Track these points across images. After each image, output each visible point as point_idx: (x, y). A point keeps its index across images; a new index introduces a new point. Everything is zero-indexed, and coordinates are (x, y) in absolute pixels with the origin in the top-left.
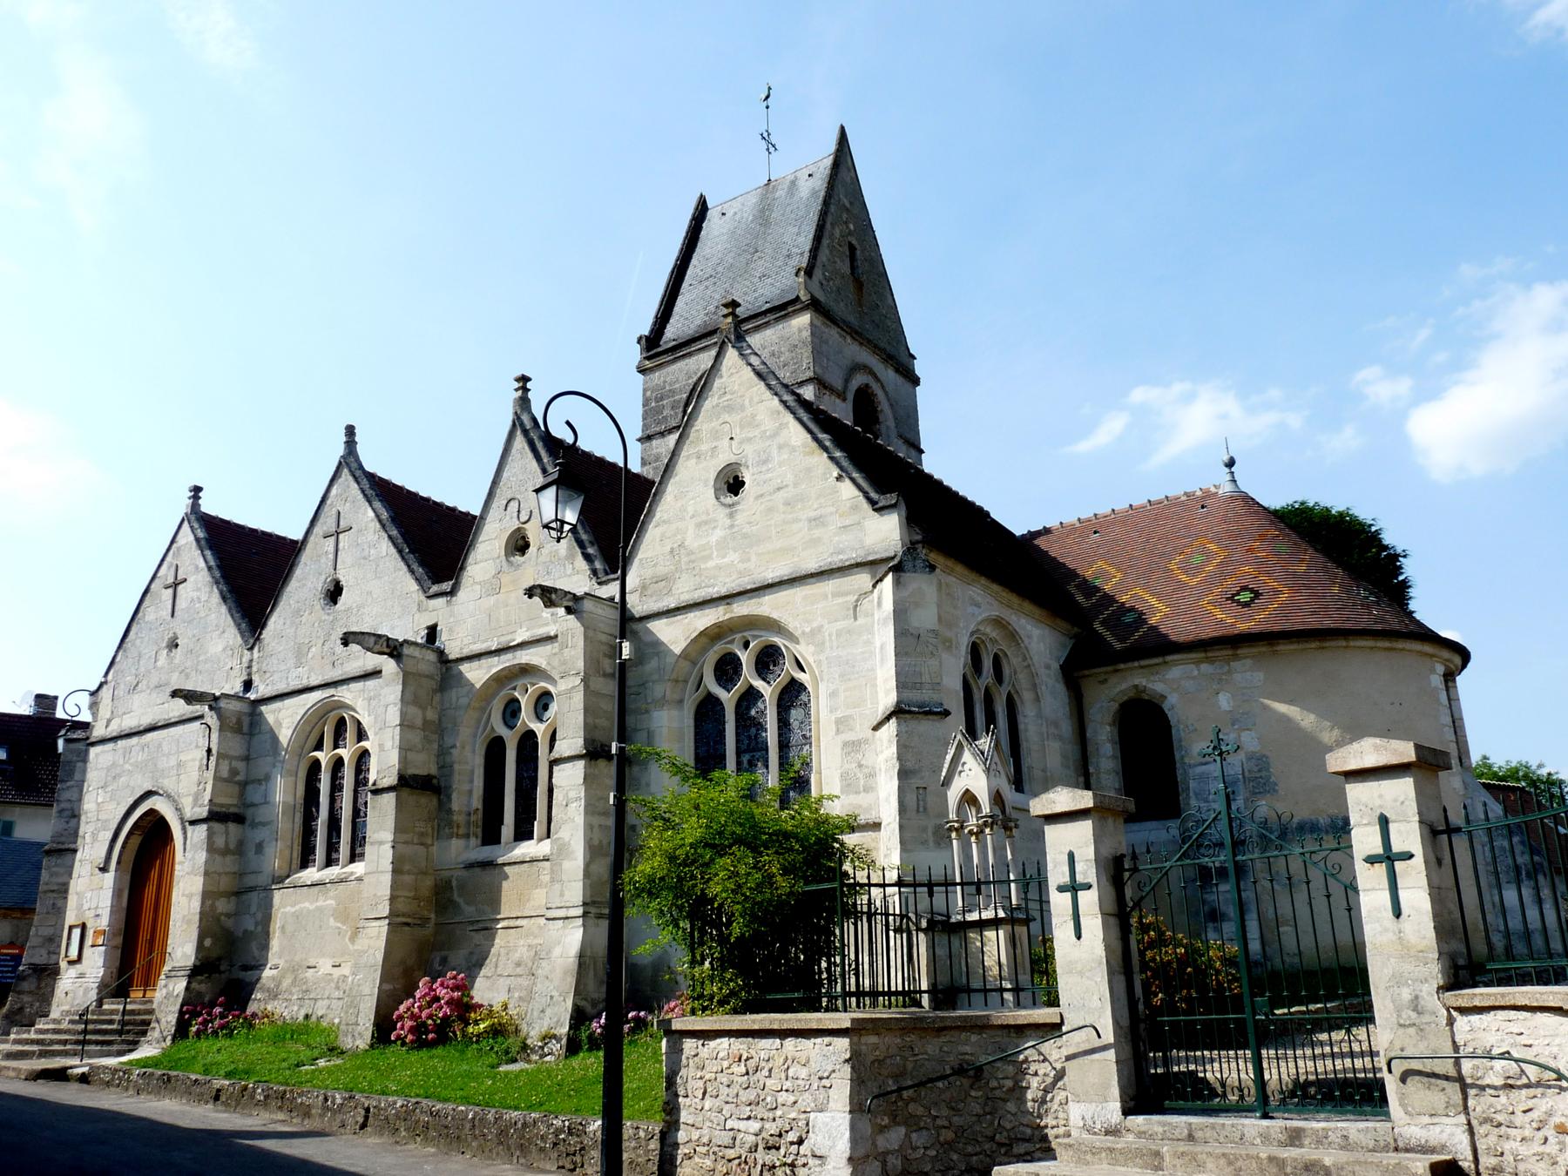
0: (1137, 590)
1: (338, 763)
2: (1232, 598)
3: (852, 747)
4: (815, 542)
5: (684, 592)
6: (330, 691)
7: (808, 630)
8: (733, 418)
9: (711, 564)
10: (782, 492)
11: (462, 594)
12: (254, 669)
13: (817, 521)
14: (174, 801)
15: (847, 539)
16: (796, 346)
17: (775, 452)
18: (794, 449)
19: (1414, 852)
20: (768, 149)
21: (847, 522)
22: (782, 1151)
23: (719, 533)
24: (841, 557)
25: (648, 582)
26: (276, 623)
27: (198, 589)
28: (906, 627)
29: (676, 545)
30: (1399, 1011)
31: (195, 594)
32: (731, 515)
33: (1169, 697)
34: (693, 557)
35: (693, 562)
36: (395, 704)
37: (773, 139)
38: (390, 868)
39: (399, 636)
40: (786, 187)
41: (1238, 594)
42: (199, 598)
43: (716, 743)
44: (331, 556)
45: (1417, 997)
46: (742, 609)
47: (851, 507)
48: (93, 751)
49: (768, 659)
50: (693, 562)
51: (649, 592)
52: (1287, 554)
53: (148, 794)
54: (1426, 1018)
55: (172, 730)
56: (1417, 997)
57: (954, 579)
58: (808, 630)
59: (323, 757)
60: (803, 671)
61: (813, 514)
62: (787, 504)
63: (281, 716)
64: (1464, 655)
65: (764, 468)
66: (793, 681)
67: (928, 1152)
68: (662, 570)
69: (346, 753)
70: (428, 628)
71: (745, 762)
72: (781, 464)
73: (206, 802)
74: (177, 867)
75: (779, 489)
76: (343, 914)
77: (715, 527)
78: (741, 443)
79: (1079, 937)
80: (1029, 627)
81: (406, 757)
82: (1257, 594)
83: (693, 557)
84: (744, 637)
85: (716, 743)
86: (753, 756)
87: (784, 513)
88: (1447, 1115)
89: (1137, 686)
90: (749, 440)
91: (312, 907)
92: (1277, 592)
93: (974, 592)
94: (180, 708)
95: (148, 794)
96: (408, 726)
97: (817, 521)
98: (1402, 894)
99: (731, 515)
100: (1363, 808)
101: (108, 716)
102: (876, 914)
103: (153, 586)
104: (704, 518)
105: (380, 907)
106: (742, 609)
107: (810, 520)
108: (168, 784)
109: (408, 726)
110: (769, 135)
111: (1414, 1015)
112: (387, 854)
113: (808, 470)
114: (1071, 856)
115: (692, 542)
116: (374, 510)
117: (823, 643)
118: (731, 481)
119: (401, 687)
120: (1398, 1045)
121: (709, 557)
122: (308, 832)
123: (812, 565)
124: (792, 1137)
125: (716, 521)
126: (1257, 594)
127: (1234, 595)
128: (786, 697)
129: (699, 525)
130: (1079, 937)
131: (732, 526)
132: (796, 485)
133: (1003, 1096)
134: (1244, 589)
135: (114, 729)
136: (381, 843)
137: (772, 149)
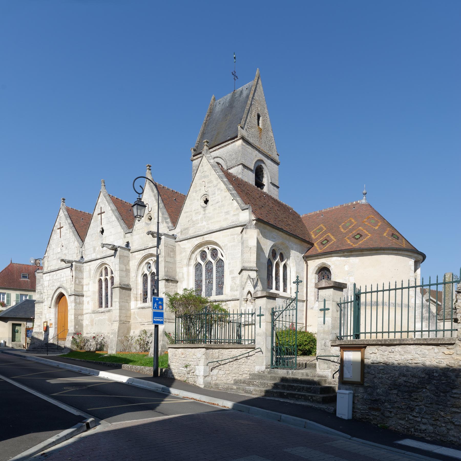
0: (329, 234)
1: (106, 280)
2: (354, 237)
3: (233, 278)
4: (226, 219)
5: (191, 233)
6: (103, 260)
7: (223, 245)
8: (206, 180)
9: (199, 225)
10: (218, 203)
11: (134, 232)
12: (83, 254)
13: (227, 213)
14: (66, 290)
15: (234, 218)
16: (236, 152)
17: (216, 190)
18: (222, 190)
19: (330, 308)
20: (234, 79)
21: (235, 213)
22: (190, 374)
23: (201, 216)
24: (233, 224)
25: (182, 230)
26: (87, 239)
27: (67, 230)
28: (247, 245)
29: (190, 219)
30: (321, 346)
31: (66, 231)
32: (204, 211)
33: (331, 266)
34: (194, 223)
35: (194, 224)
36: (118, 264)
37: (236, 74)
38: (119, 308)
39: (117, 244)
40: (239, 93)
41: (356, 236)
42: (67, 233)
43: (200, 277)
44: (100, 221)
45: (325, 343)
46: (207, 238)
47: (236, 209)
48: (439, 290)
49: (214, 253)
50: (194, 224)
51: (183, 233)
52: (374, 223)
53: (59, 288)
54: (326, 348)
55: (64, 270)
56: (325, 343)
57: (267, 231)
58: (223, 245)
59: (103, 278)
60: (223, 256)
61: (226, 211)
62: (219, 207)
63: (91, 267)
64: (424, 257)
65: (213, 196)
66: (220, 259)
67: (223, 376)
68: (186, 226)
69: (108, 277)
70: (127, 242)
71: (208, 282)
72: (218, 195)
73: (73, 290)
74: (68, 307)
75: (217, 203)
76: (110, 320)
77: (200, 214)
78: (207, 188)
79: (260, 327)
80: (292, 245)
81: (121, 279)
82: (361, 236)
83: (194, 223)
84: (208, 247)
85: (200, 277)
86: (210, 280)
87: (218, 210)
88: (327, 369)
89: (323, 263)
90: (210, 187)
91: (102, 318)
92: (367, 235)
93: (274, 234)
94: (63, 265)
95: (59, 288)
96: (121, 270)
97: (227, 213)
98: (326, 318)
99: (204, 211)
100: (321, 297)
101: (47, 266)
102: (235, 323)
103: (54, 229)
104: (197, 211)
105: (117, 318)
106: (207, 238)
107: (225, 213)
108: (64, 285)
109: (121, 270)
110: (235, 73)
111: (324, 347)
112: (117, 304)
113: (225, 197)
114: (260, 307)
115: (194, 219)
116: (110, 207)
117: (227, 249)
118: (205, 200)
119: (119, 259)
120: (320, 353)
121: (199, 223)
122: (101, 298)
123: (225, 225)
124: (192, 371)
125: (200, 212)
126: (361, 236)
127: (355, 236)
128: (270, 264)
129: (196, 213)
130: (260, 327)
131: (204, 214)
132: (222, 202)
133: (242, 364)
134: (358, 234)
135: (49, 269)
136: (116, 302)
137: (236, 78)
